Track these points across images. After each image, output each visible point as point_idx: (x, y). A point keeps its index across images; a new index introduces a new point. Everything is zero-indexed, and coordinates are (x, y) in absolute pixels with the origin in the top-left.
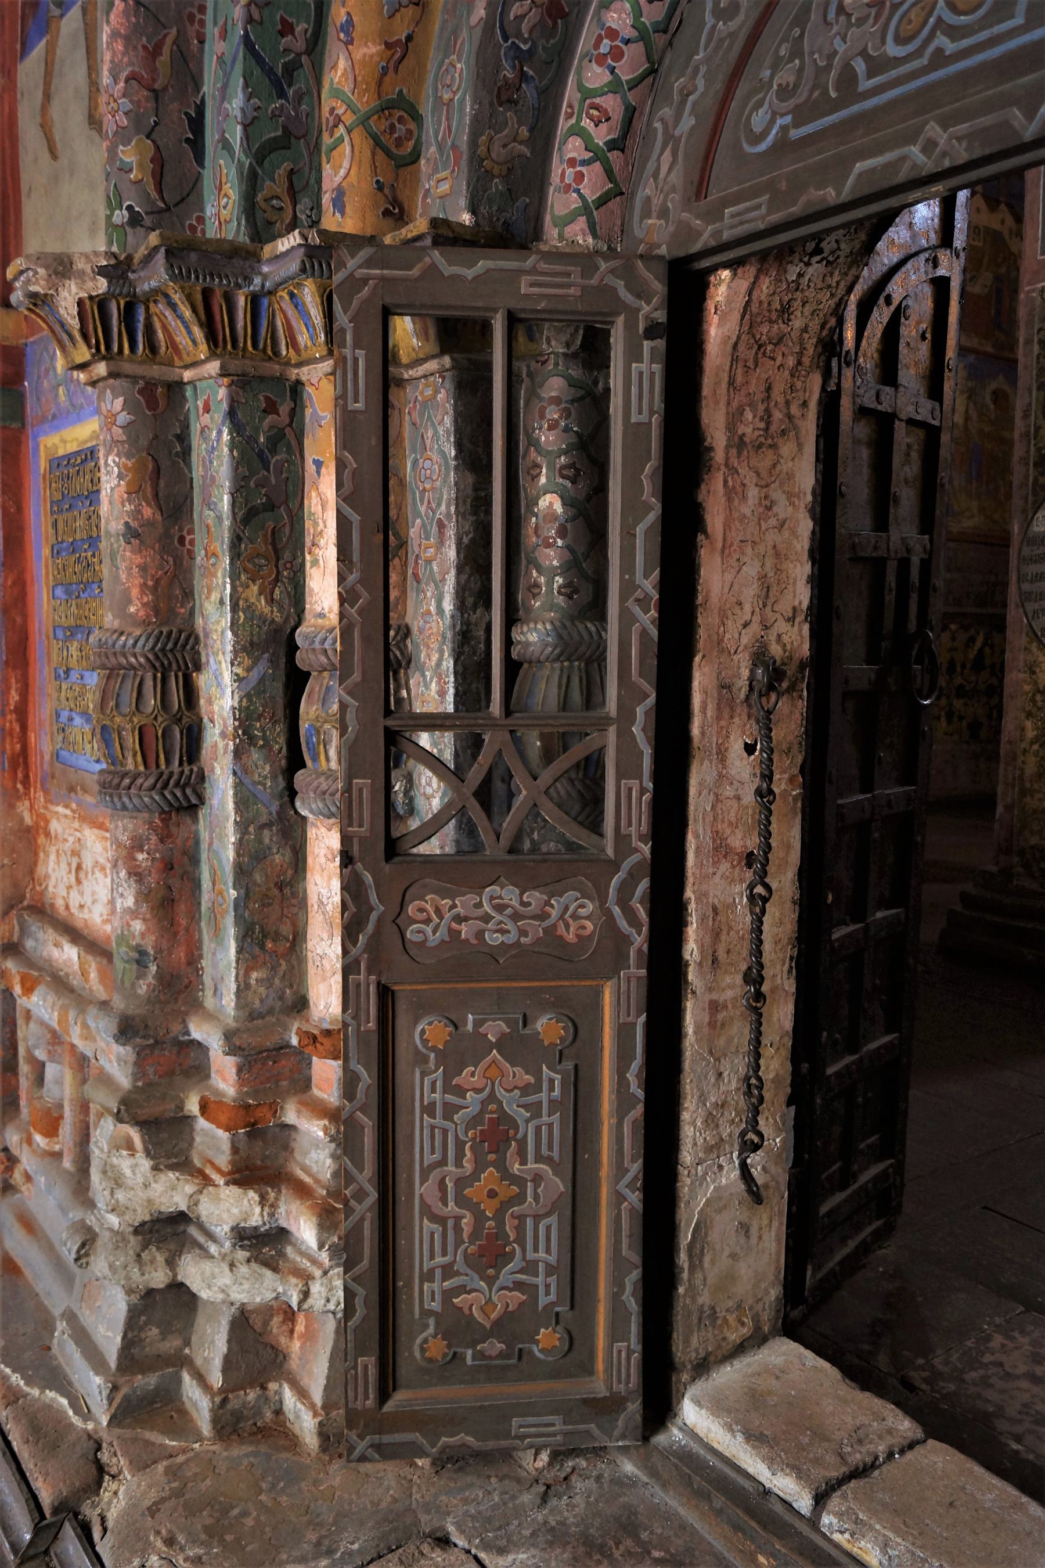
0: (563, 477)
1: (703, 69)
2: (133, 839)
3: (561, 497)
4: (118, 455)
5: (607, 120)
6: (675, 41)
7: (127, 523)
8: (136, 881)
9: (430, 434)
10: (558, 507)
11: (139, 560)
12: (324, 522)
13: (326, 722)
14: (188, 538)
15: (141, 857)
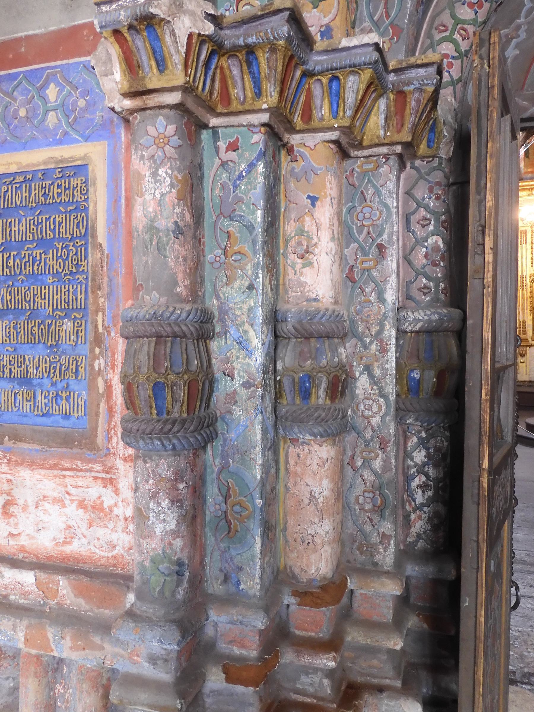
0: (443, 227)
1: (524, 28)
2: (175, 473)
3: (443, 239)
4: (171, 168)
5: (468, 39)
6: (499, 9)
7: (176, 222)
8: (177, 507)
9: (371, 191)
10: (441, 244)
11: (183, 252)
12: (319, 238)
13: (320, 372)
14: (202, 240)
15: (181, 486)
